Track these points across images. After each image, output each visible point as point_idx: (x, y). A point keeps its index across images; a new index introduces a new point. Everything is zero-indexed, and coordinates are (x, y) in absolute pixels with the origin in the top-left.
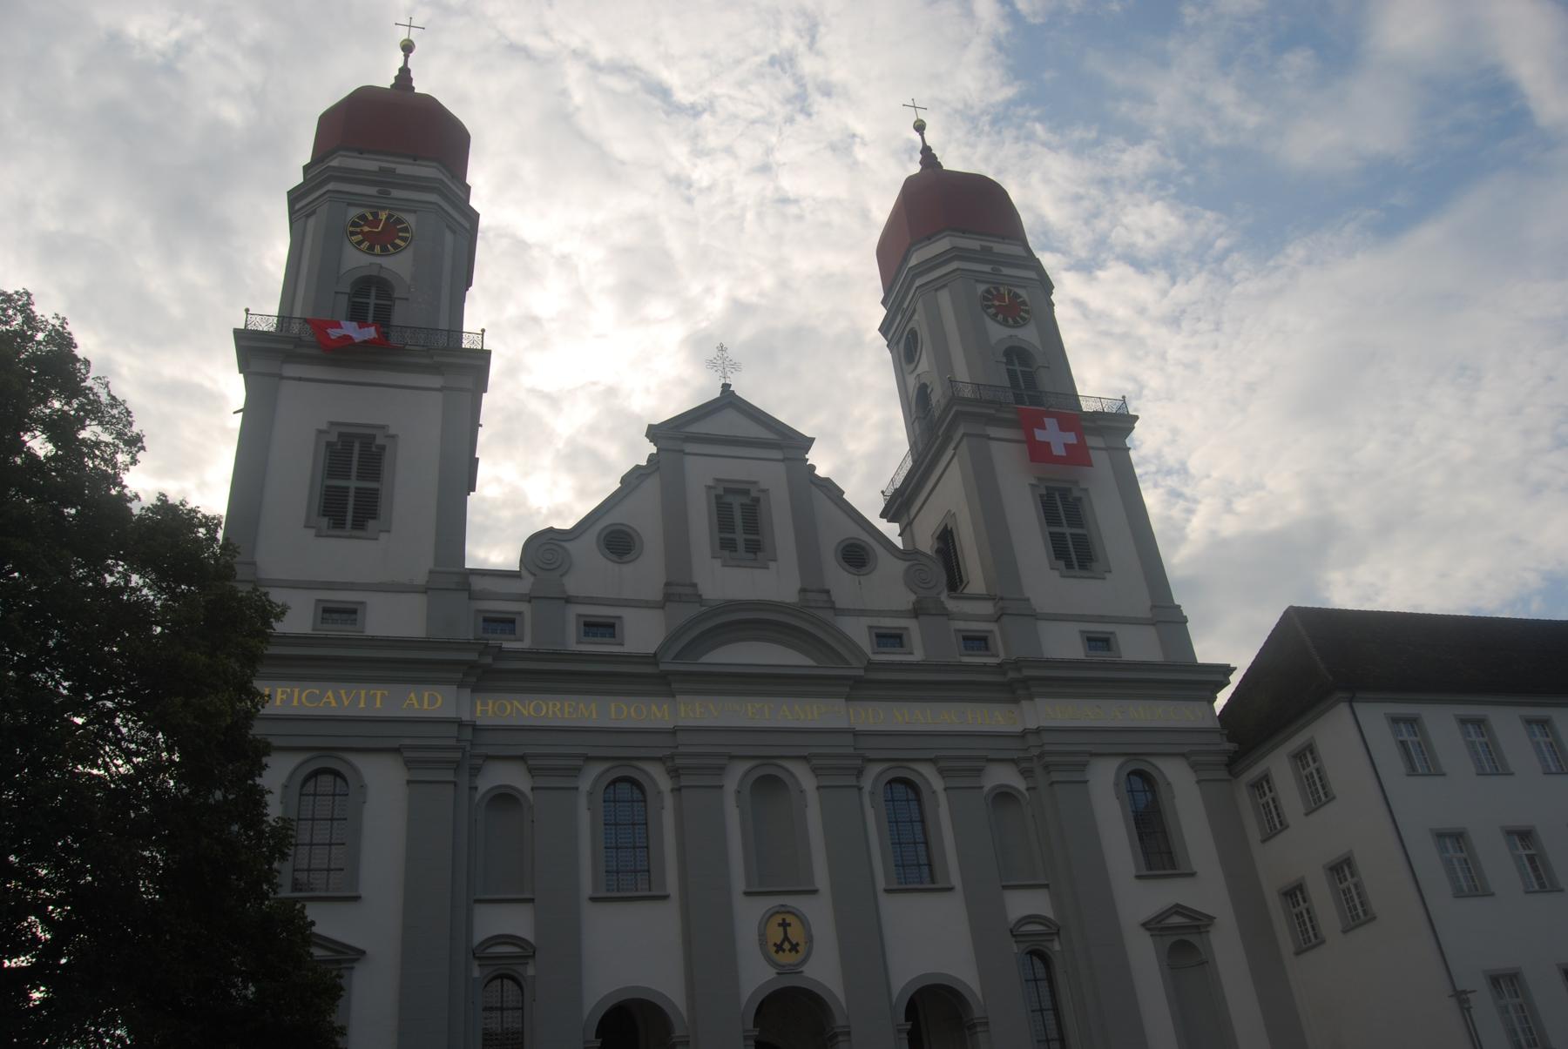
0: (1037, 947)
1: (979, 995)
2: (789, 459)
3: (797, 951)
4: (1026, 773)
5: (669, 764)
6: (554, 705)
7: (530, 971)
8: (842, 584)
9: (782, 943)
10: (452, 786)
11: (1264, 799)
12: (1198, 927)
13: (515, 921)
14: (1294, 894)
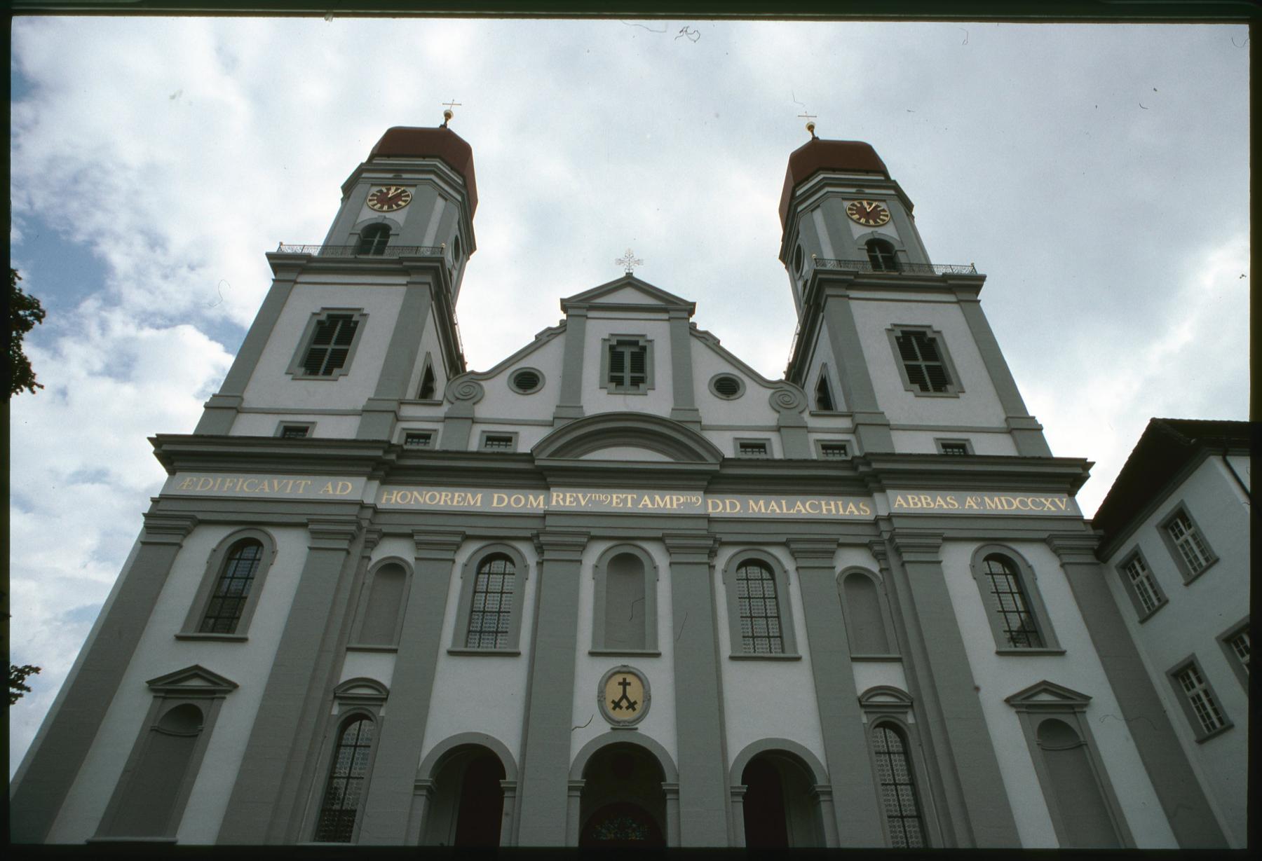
0: (887, 719)
1: (823, 761)
2: (672, 318)
3: (634, 709)
4: (879, 556)
5: (535, 541)
6: (558, 496)
7: (382, 712)
8: (712, 409)
9: (621, 700)
10: (344, 553)
11: (1138, 579)
12: (1072, 707)
13: (379, 668)
14: (1186, 673)
